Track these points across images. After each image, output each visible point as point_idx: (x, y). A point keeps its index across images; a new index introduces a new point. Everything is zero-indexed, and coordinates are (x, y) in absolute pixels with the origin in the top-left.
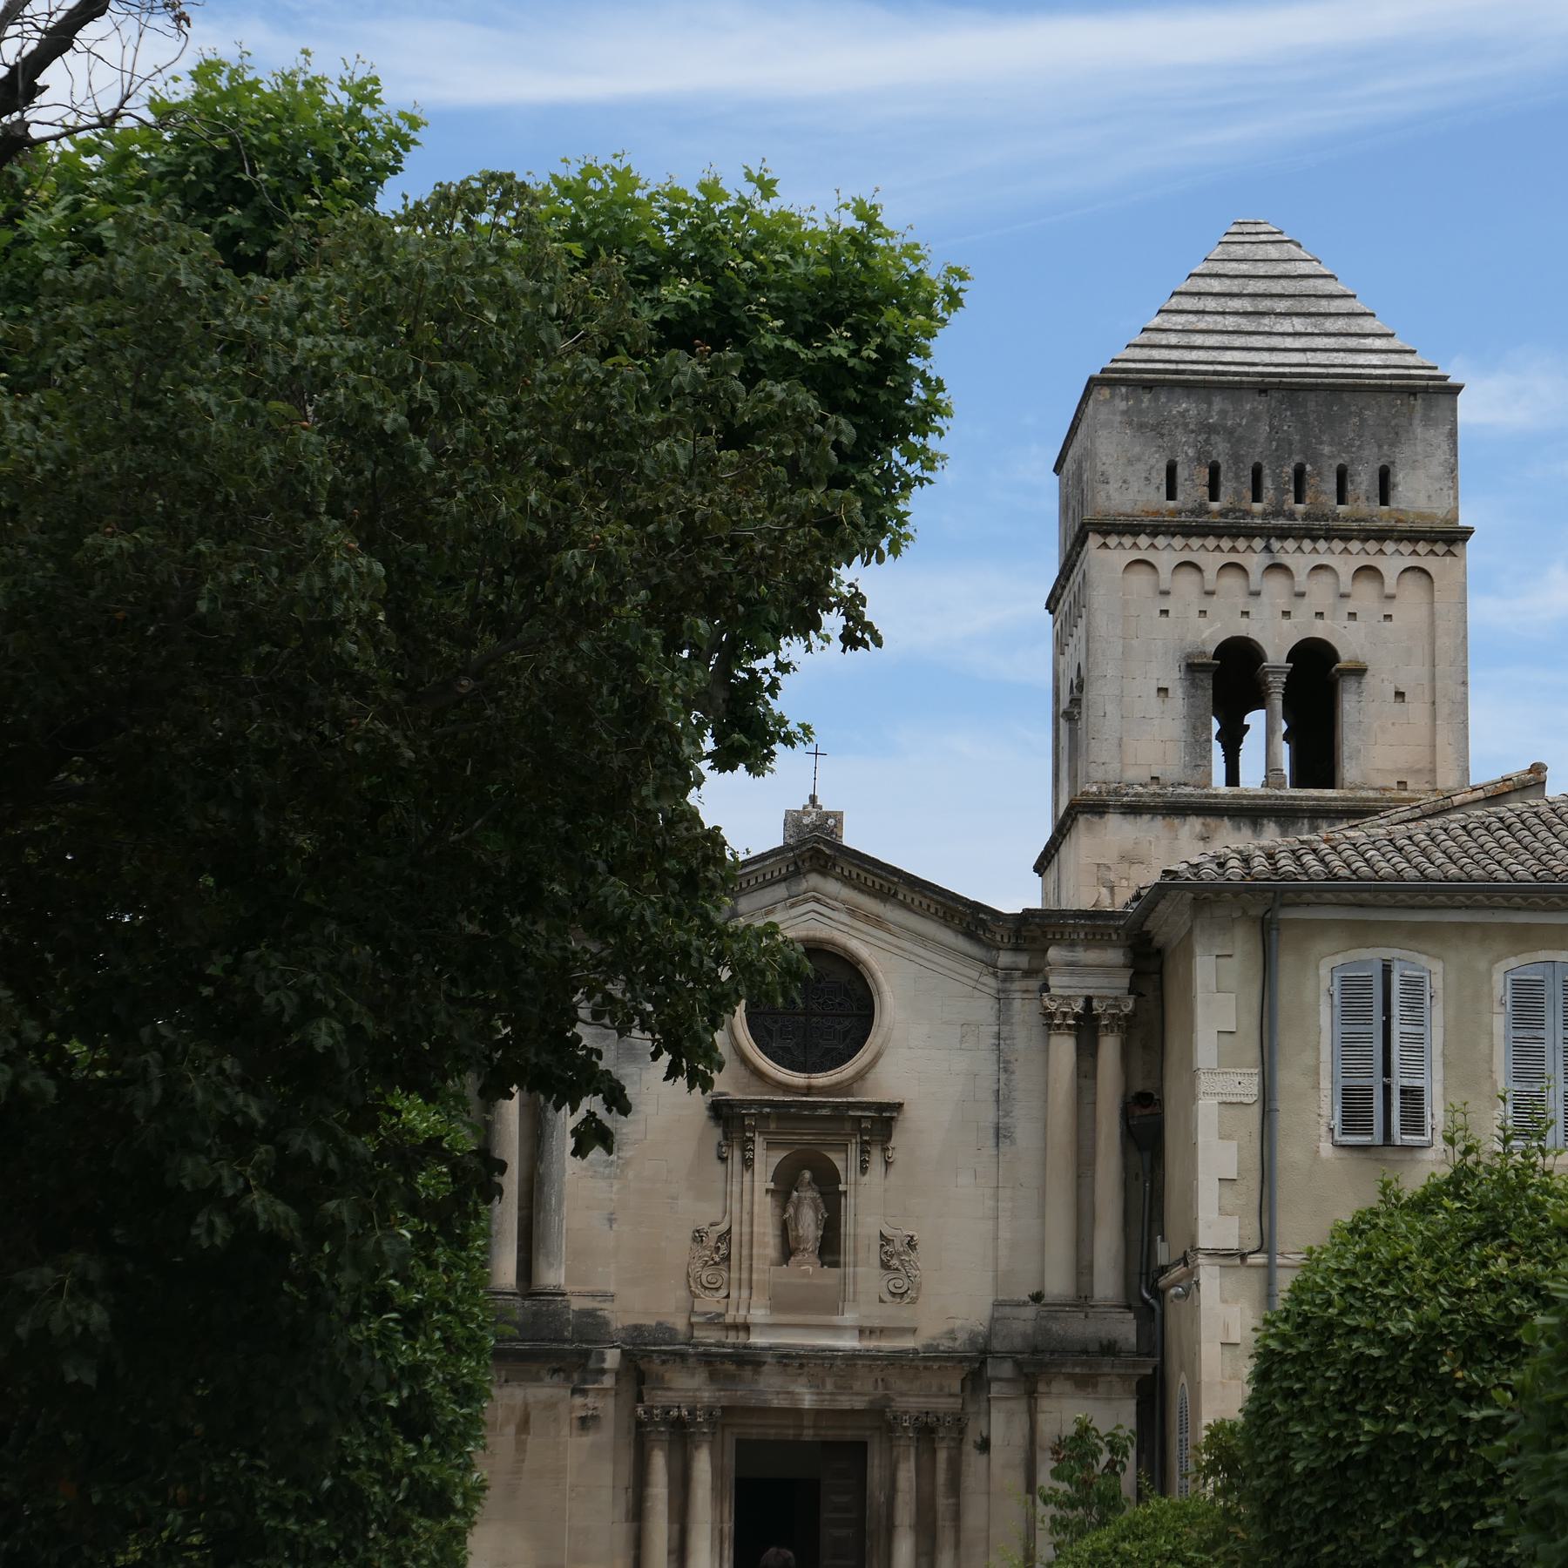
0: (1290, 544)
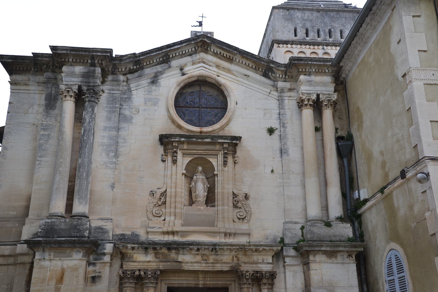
0: (329, 47)
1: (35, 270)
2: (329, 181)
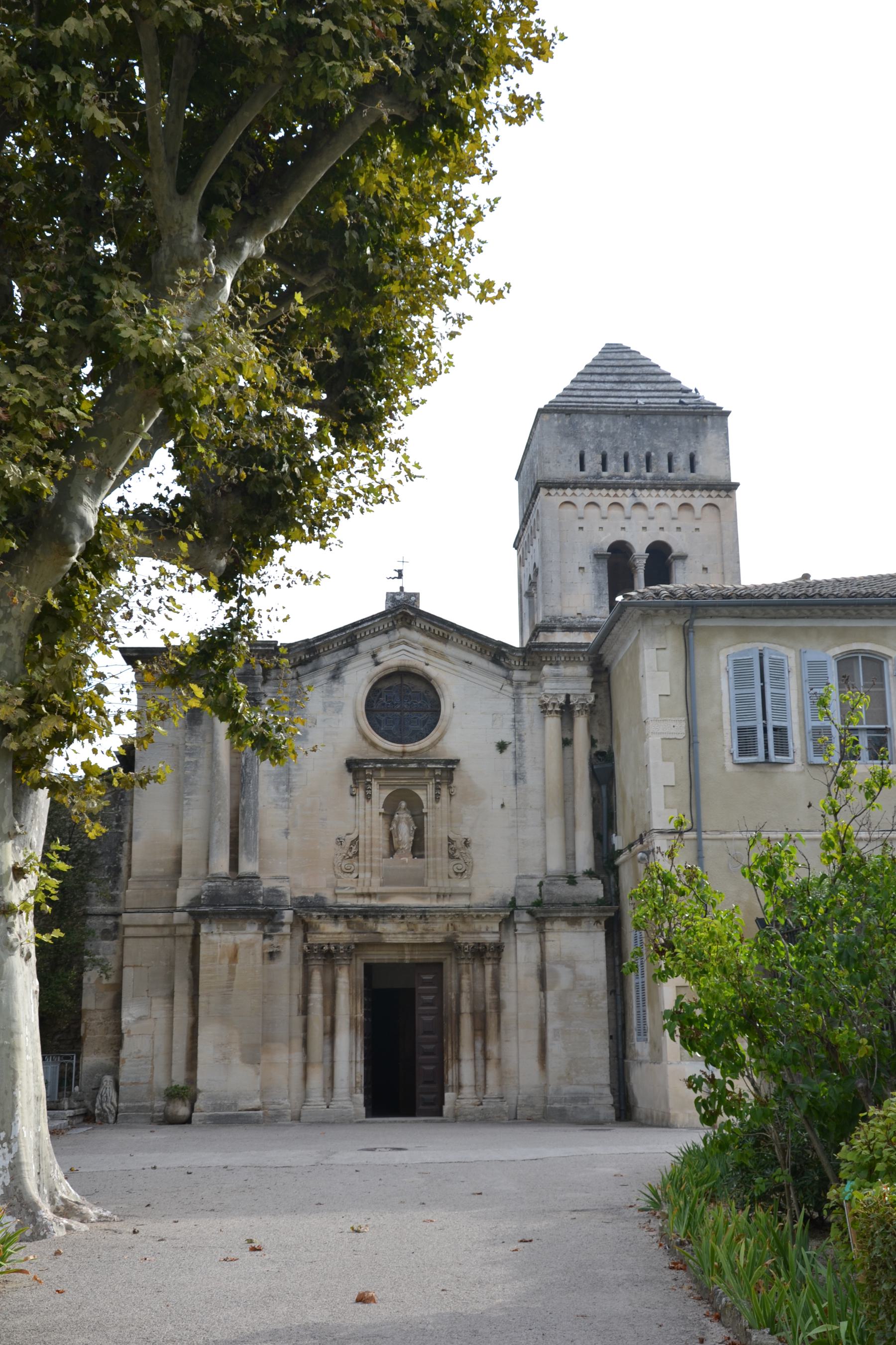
0: (645, 492)
1: (203, 947)
2: (577, 822)
